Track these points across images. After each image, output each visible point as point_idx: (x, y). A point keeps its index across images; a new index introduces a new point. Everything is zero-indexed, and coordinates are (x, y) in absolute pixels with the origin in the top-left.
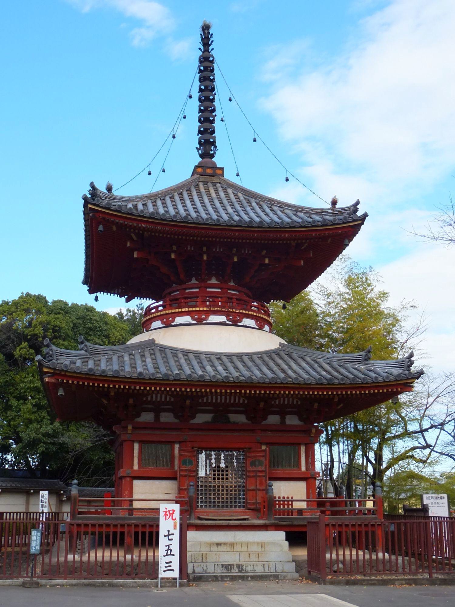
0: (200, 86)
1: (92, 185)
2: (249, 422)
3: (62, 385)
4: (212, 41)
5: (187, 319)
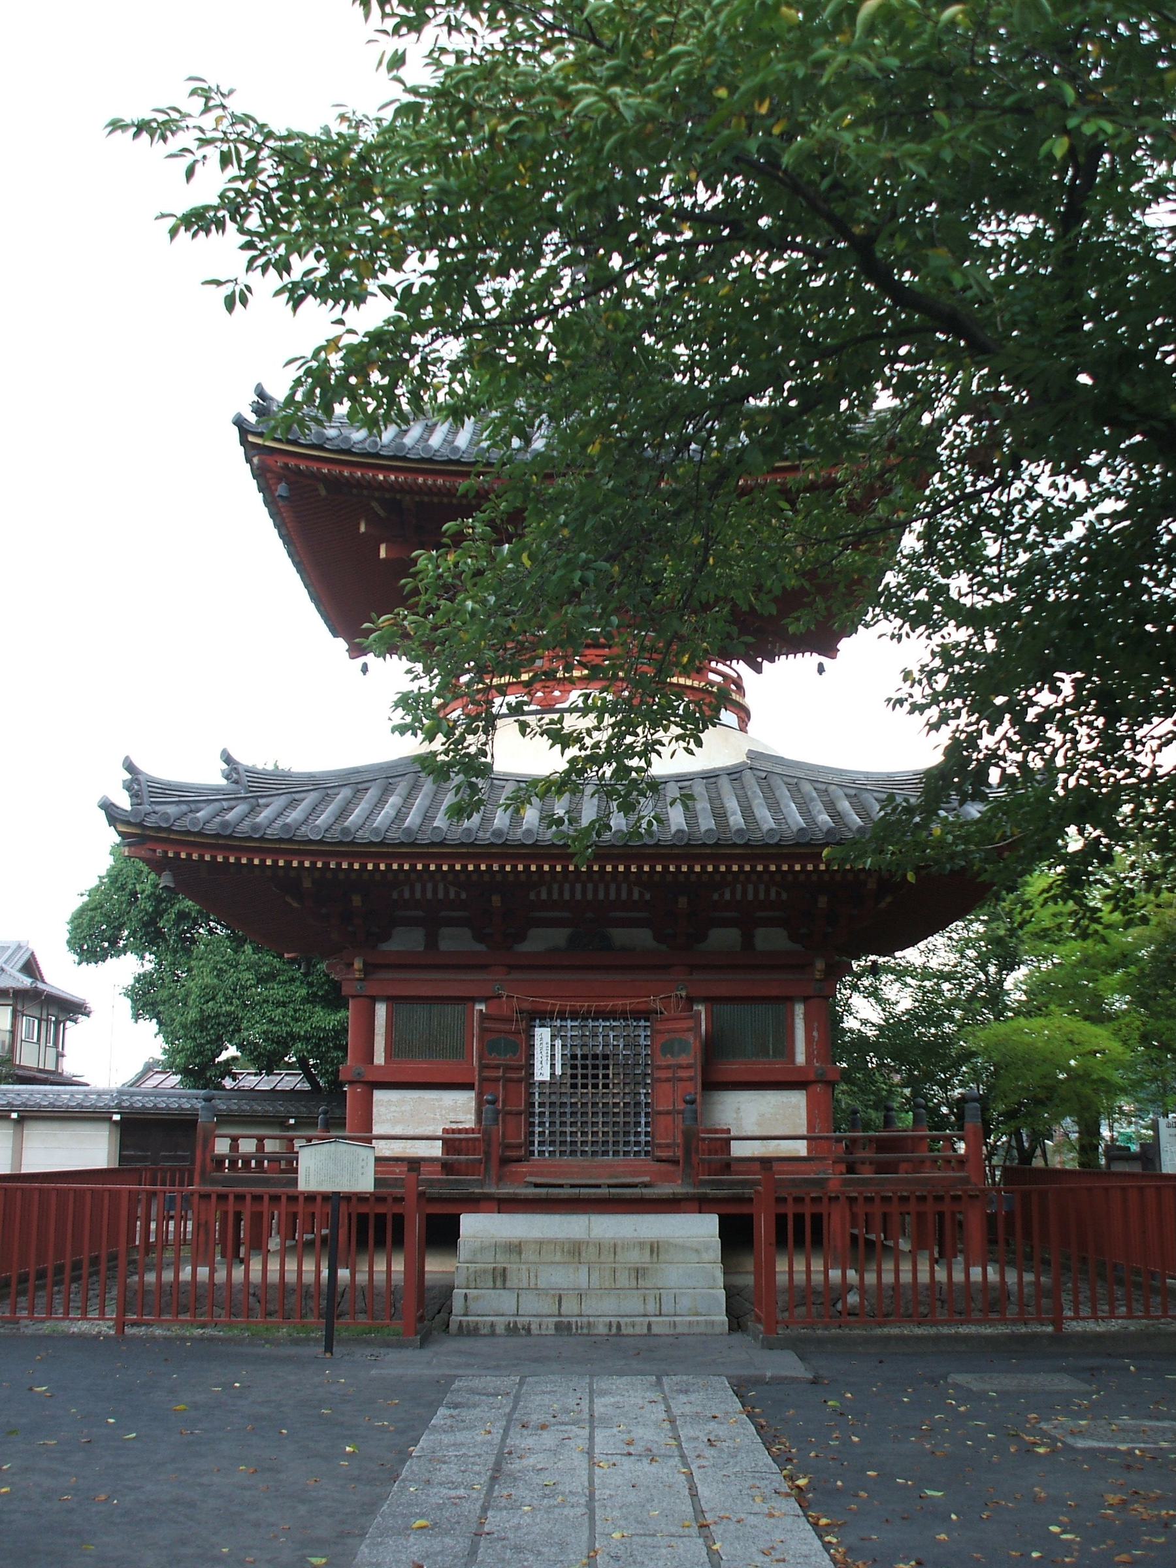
1: (261, 393)
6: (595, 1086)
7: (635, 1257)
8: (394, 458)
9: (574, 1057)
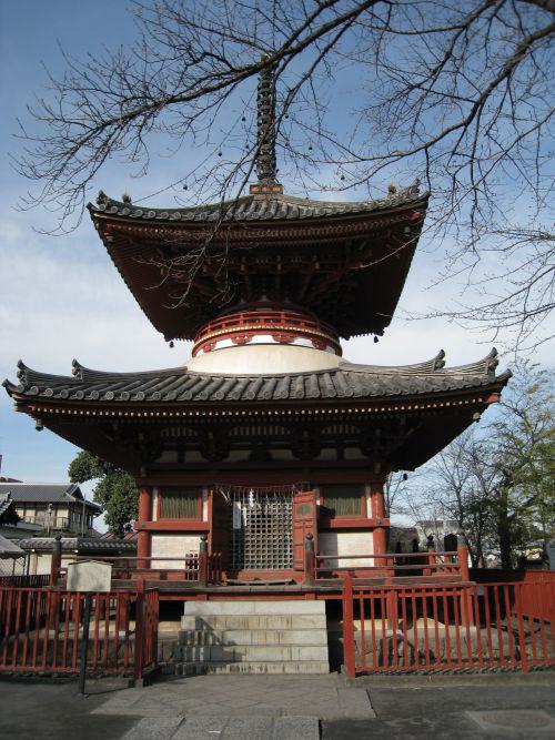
5: (268, 338)
6: (264, 531)
7: (278, 625)
9: (253, 516)
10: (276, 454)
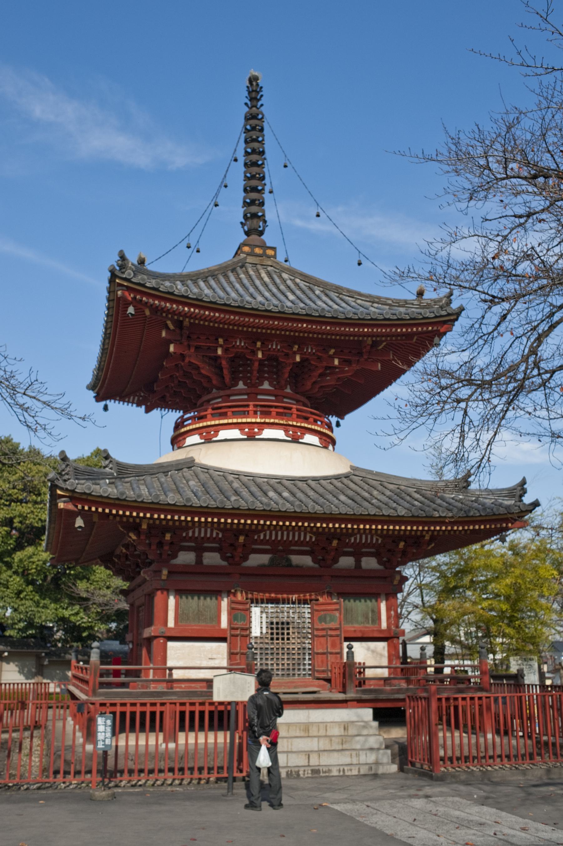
0: (245, 149)
2: (317, 566)
3: (81, 513)
4: (262, 96)
5: (280, 434)
6: (283, 639)
8: (196, 299)
10: (296, 559)
